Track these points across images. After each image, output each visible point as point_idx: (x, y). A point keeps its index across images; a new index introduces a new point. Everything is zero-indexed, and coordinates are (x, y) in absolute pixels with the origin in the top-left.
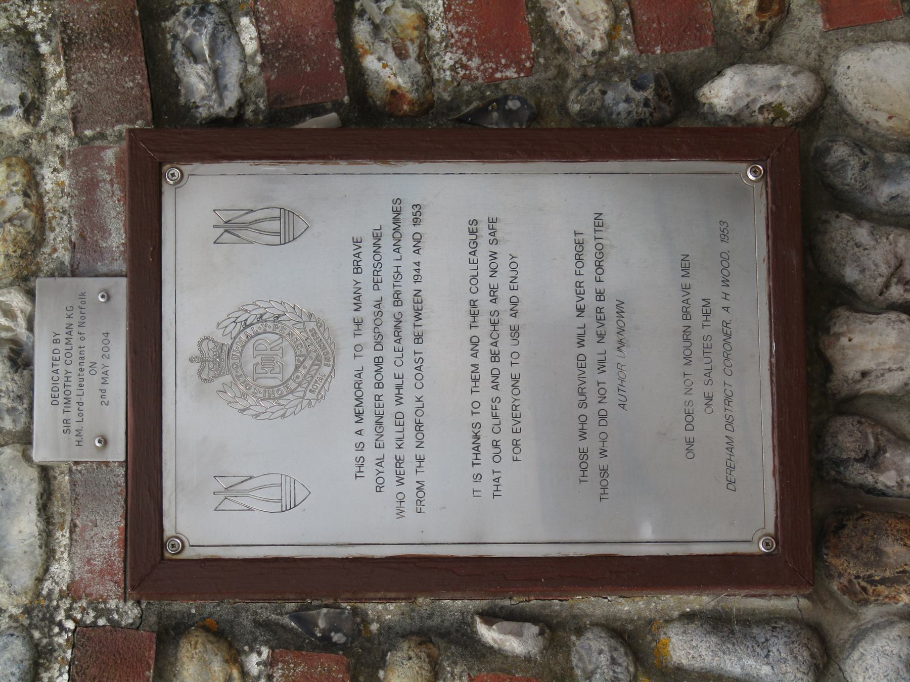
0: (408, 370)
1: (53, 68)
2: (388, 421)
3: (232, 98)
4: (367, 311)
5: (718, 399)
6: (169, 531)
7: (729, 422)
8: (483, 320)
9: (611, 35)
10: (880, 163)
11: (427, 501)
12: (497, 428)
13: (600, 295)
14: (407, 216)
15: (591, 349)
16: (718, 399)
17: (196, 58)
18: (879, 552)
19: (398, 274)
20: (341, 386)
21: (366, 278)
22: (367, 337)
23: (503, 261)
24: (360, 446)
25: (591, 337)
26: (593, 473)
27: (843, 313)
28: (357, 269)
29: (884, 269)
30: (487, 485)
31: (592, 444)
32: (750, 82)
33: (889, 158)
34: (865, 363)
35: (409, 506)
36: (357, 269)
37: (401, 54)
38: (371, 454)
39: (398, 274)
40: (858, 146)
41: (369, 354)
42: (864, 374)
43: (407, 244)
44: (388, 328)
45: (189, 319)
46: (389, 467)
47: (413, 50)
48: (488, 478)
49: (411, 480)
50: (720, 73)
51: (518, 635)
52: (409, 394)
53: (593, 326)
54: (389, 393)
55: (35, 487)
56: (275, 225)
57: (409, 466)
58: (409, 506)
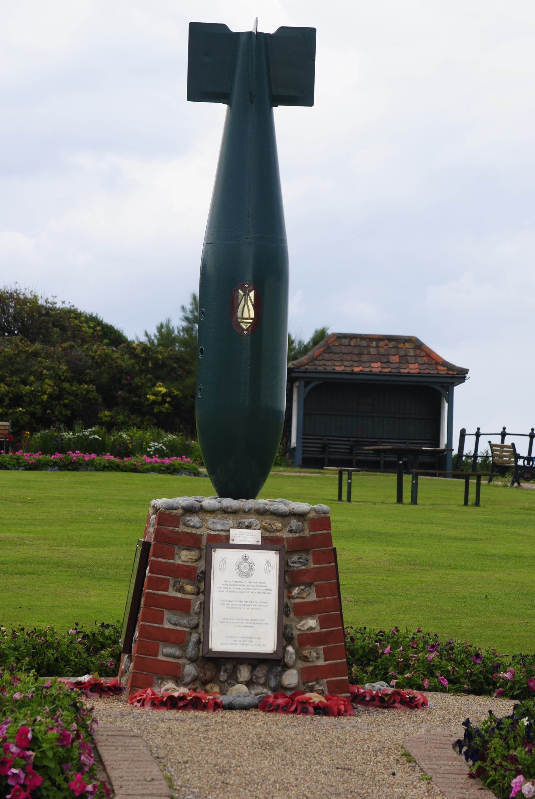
0: (242, 590)
1: (297, 535)
2: (234, 586)
3: (291, 564)
4: (252, 584)
5: (235, 642)
6: (217, 549)
7: (232, 644)
8: (251, 603)
9: (300, 630)
10: (277, 676)
11: (231, 600)
12: (232, 605)
13: (254, 623)
14: (268, 591)
15: (245, 622)
16: (235, 642)
17: (299, 559)
18: (209, 670)
19: (259, 589)
20: (239, 579)
21: (258, 584)
22: (248, 584)
23: (260, 607)
24: (230, 582)
25: (246, 621)
26: (224, 620)
27: (251, 668)
28: (260, 583)
29: (258, 675)
30: (222, 603)
31: (229, 621)
32: (291, 654)
33: (278, 678)
34: (242, 671)
35: (220, 589)
36: (260, 583)
37: (298, 594)
38: (228, 583)
39: (259, 589)
40: (280, 672)
41: (246, 584)
42: (240, 670)
43: (264, 591)
44: (250, 587)
45: (252, 554)
46: (226, 586)
47: (299, 596)
48: (224, 603)
49: (224, 590)
50: (294, 649)
51: (198, 608)
52: (239, 590)
53: (248, 622)
54: (239, 587)
55: (226, 529)
56: (268, 569)
57: (226, 590)
58: (220, 589)
